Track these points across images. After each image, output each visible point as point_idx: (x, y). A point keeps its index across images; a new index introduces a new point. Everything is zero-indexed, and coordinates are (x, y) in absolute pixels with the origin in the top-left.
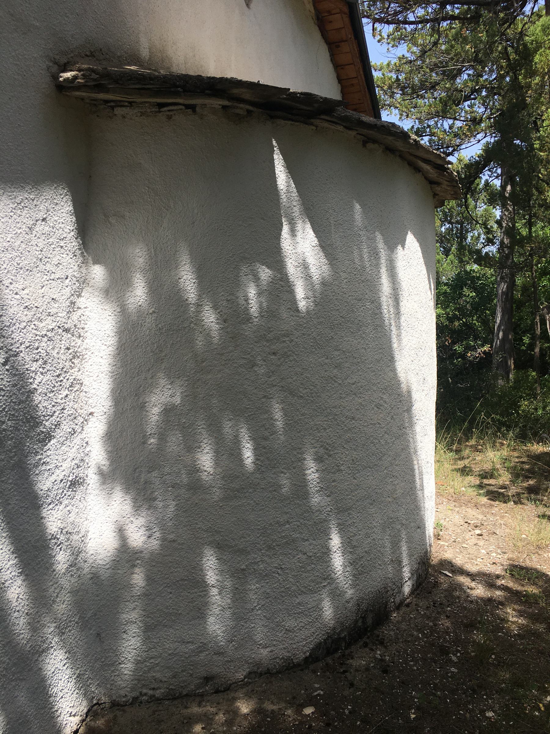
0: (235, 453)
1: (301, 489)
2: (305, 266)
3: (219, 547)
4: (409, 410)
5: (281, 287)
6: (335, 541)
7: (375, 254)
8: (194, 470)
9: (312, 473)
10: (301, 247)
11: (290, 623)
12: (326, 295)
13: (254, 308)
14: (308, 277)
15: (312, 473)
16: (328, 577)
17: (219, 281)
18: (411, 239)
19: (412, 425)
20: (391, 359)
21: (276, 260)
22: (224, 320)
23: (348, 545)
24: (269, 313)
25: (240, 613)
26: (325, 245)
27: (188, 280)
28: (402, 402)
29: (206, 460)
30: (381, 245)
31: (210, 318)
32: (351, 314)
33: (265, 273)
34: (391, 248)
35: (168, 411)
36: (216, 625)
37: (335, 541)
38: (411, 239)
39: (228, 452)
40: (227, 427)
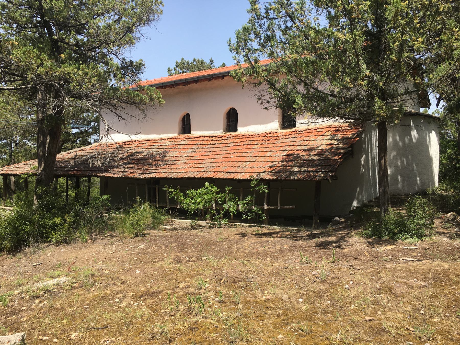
0: (404, 163)
1: (413, 170)
2: (415, 136)
3: (401, 176)
4: (432, 161)
5: (411, 139)
6: (418, 179)
7: (426, 134)
8: (398, 165)
9: (415, 166)
10: (414, 133)
11: (411, 189)
12: (418, 140)
13: (407, 142)
14: (415, 138)
15: (415, 166)
16: (417, 183)
17: (402, 139)
18: (433, 132)
19: (433, 164)
20: (429, 152)
21: (410, 135)
22: (403, 144)
23: (420, 180)
24: (409, 143)
25: (403, 186)
26: (418, 133)
27: (398, 138)
28: (430, 160)
29: (399, 163)
30: (427, 133)
31: (401, 144)
32: (423, 145)
33: (409, 137)
34: (429, 133)
35: (394, 156)
36: (400, 186)
37: (418, 179)
38: (433, 132)
39: (402, 162)
40: (403, 159)
